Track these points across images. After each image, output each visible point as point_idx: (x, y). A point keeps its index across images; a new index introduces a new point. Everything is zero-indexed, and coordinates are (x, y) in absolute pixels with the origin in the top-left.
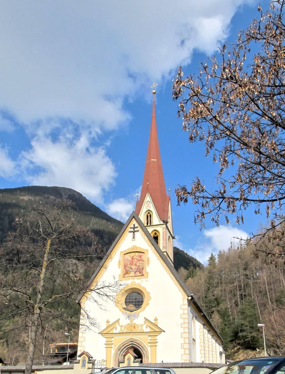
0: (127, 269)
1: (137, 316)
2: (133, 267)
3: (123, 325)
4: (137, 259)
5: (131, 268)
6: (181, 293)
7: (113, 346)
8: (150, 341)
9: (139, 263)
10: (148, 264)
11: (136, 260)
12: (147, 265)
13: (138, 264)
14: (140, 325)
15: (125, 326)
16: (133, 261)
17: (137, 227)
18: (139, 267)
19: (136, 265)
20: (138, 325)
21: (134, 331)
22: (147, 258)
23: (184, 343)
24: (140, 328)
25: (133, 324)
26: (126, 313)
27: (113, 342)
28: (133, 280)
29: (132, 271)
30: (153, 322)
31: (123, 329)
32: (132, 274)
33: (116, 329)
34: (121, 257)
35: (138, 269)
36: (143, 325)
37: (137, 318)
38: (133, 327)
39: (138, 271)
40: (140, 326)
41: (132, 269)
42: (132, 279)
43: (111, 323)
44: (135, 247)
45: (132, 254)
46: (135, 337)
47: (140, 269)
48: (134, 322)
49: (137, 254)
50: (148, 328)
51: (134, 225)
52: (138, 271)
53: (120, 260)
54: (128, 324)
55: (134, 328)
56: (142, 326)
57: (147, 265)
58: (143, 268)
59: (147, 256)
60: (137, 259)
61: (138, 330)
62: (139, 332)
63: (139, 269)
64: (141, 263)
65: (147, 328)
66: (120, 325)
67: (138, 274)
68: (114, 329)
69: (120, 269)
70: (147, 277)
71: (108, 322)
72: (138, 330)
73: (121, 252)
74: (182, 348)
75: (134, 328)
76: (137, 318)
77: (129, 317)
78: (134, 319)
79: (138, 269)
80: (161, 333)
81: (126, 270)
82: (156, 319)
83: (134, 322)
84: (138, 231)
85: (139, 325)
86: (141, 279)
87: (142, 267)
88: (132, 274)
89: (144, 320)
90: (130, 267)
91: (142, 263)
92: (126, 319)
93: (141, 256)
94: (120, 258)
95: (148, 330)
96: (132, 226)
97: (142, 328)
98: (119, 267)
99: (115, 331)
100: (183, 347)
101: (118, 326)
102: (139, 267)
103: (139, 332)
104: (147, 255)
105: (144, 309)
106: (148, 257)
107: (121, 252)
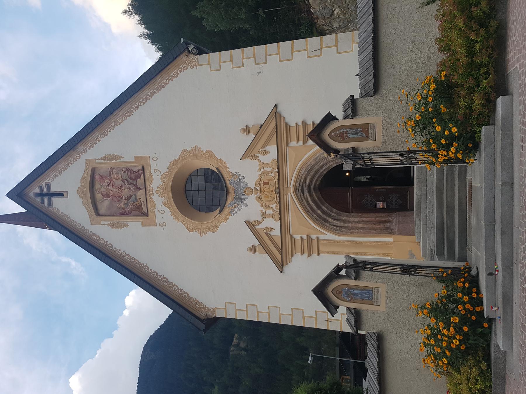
0: (129, 208)
1: (239, 179)
2: (126, 192)
3: (262, 211)
4: (108, 185)
5: (128, 199)
6: (180, 71)
7: (314, 237)
8: (301, 143)
9: (117, 179)
10: (116, 157)
11: (110, 188)
12: (118, 161)
13: (119, 182)
14: (260, 170)
15: (262, 206)
16: (111, 194)
17: (41, 188)
18: (126, 180)
19: (122, 187)
20: (260, 176)
21: (274, 183)
22: (103, 161)
23: (307, 49)
24: (269, 169)
25: (258, 188)
26: (231, 205)
27: (305, 237)
28: (154, 192)
29: (135, 195)
30: (252, 136)
31: (269, 212)
32: (140, 194)
33: (271, 229)
34: (103, 223)
35: (131, 181)
36: (260, 161)
37: (244, 177)
38: (265, 186)
39: (134, 182)
40: (262, 170)
41: (131, 196)
42: (153, 195)
43: (257, 243)
44: (80, 192)
45: (98, 196)
46: (291, 181)
47: (131, 178)
48: (252, 185)
49: (97, 186)
50: (268, 148)
51: (37, 195)
52: (134, 182)
53: (109, 225)
54: (259, 198)
55: (267, 183)
56: (262, 165)
57: (118, 161)
58: (127, 170)
59: (101, 161)
60: (108, 185)
61: (273, 175)
62: (278, 172)
63: (128, 179)
64: (116, 176)
65: (267, 152)
66: (260, 219)
67: (140, 181)
68: (272, 233)
69: (130, 223)
70: (146, 158)
71: (253, 249)
72: (273, 175)
73: (93, 222)
74: (321, 55)
75: (267, 183)
76: (244, 177)
77: (241, 199)
78: (247, 184)
79: (131, 181)
80: (281, 116)
81: (132, 209)
82: (247, 130)
83: (252, 185)
84: (48, 185)
85: (260, 173)
86: (152, 172)
87: (125, 172)
88: (140, 194)
89: (248, 160)
90: (126, 201)
91: (117, 174)
92: (247, 205)
93: (102, 177)
94: (105, 224)
95: (272, 149)
96: (39, 199)
97: (268, 165)
98: (126, 225)
99: (276, 233)
100: (318, 53)
101: (263, 225)
102: (126, 180)
103: (277, 170)
104: (97, 161)
105: (221, 161)
106: (102, 159)
107: (93, 222)
